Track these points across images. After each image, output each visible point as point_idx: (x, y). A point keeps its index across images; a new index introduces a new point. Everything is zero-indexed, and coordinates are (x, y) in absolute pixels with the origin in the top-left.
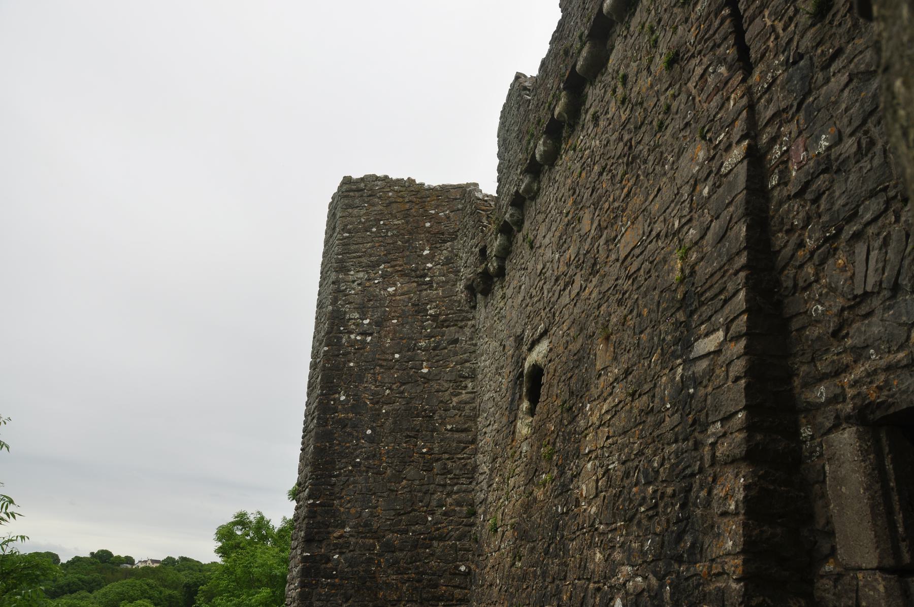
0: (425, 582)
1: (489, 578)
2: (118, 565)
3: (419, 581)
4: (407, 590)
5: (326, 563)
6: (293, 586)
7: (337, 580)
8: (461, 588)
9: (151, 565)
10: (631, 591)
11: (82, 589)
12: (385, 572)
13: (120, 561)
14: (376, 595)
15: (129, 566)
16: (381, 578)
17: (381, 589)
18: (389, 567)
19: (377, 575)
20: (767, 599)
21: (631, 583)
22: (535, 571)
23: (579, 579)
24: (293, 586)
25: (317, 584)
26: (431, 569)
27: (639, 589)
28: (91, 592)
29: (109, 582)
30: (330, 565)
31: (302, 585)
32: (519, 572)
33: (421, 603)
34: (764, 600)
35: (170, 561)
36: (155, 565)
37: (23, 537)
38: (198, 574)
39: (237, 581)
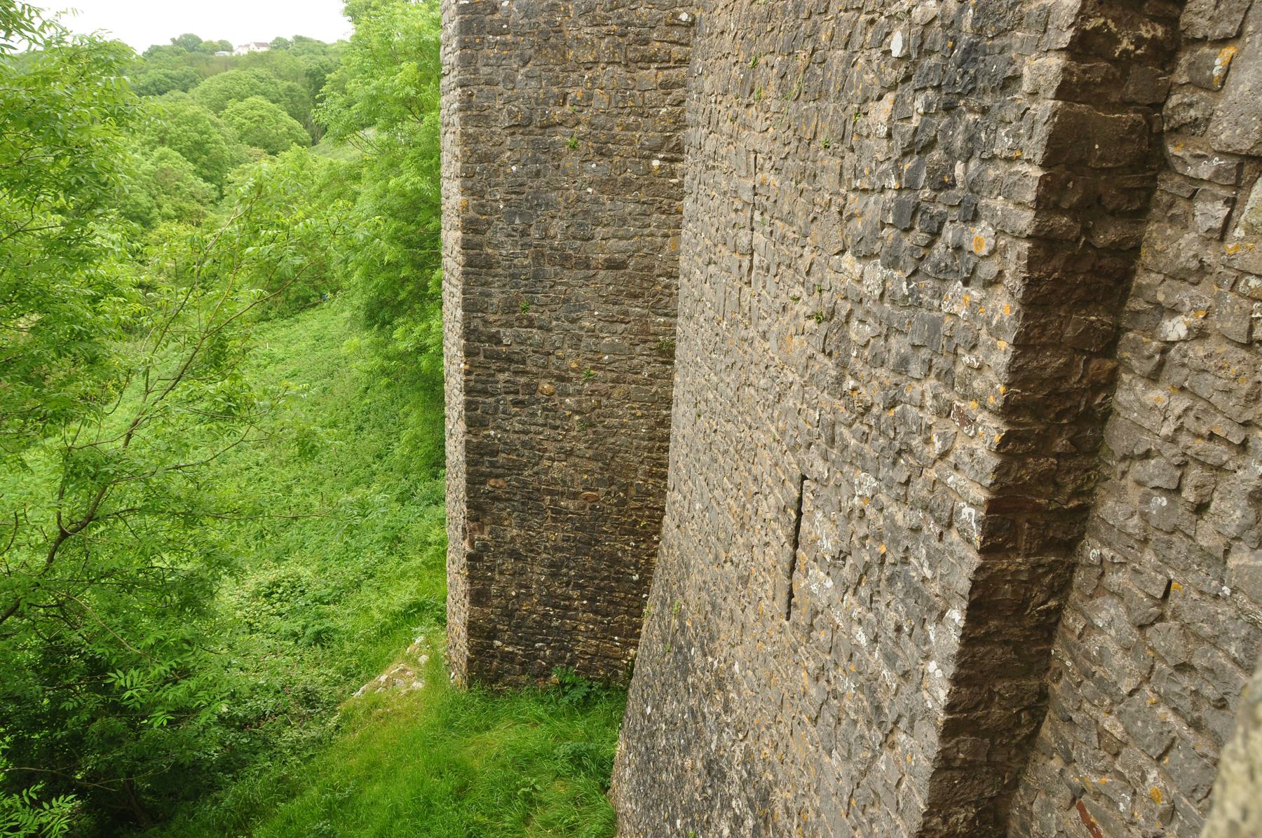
0: (631, 36)
1: (720, 23)
2: (212, 53)
3: (623, 35)
4: (607, 48)
5: (493, 13)
6: (448, 49)
7: (509, 37)
8: (682, 44)
9: (256, 50)
10: (918, 20)
11: (173, 88)
12: (575, 23)
13: (212, 48)
14: (563, 56)
15: (227, 54)
16: (570, 32)
17: (570, 47)
18: (580, 16)
19: (564, 28)
20: (1109, 21)
21: (919, 9)
22: (785, 5)
23: (846, 10)
24: (448, 49)
25: (482, 42)
26: (639, 18)
27: (930, 17)
28: (185, 90)
29: (205, 76)
30: (497, 16)
31: (464, 46)
32: (762, 9)
33: (626, 65)
34: (1105, 23)
35: (280, 44)
36: (265, 49)
37: (74, 11)
38: (322, 58)
39: (373, 56)
